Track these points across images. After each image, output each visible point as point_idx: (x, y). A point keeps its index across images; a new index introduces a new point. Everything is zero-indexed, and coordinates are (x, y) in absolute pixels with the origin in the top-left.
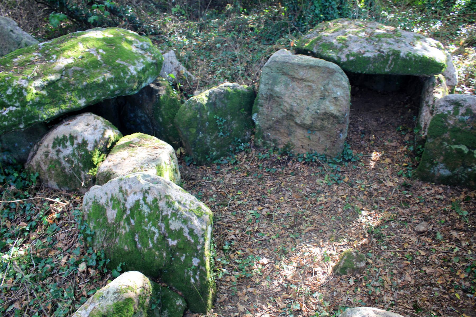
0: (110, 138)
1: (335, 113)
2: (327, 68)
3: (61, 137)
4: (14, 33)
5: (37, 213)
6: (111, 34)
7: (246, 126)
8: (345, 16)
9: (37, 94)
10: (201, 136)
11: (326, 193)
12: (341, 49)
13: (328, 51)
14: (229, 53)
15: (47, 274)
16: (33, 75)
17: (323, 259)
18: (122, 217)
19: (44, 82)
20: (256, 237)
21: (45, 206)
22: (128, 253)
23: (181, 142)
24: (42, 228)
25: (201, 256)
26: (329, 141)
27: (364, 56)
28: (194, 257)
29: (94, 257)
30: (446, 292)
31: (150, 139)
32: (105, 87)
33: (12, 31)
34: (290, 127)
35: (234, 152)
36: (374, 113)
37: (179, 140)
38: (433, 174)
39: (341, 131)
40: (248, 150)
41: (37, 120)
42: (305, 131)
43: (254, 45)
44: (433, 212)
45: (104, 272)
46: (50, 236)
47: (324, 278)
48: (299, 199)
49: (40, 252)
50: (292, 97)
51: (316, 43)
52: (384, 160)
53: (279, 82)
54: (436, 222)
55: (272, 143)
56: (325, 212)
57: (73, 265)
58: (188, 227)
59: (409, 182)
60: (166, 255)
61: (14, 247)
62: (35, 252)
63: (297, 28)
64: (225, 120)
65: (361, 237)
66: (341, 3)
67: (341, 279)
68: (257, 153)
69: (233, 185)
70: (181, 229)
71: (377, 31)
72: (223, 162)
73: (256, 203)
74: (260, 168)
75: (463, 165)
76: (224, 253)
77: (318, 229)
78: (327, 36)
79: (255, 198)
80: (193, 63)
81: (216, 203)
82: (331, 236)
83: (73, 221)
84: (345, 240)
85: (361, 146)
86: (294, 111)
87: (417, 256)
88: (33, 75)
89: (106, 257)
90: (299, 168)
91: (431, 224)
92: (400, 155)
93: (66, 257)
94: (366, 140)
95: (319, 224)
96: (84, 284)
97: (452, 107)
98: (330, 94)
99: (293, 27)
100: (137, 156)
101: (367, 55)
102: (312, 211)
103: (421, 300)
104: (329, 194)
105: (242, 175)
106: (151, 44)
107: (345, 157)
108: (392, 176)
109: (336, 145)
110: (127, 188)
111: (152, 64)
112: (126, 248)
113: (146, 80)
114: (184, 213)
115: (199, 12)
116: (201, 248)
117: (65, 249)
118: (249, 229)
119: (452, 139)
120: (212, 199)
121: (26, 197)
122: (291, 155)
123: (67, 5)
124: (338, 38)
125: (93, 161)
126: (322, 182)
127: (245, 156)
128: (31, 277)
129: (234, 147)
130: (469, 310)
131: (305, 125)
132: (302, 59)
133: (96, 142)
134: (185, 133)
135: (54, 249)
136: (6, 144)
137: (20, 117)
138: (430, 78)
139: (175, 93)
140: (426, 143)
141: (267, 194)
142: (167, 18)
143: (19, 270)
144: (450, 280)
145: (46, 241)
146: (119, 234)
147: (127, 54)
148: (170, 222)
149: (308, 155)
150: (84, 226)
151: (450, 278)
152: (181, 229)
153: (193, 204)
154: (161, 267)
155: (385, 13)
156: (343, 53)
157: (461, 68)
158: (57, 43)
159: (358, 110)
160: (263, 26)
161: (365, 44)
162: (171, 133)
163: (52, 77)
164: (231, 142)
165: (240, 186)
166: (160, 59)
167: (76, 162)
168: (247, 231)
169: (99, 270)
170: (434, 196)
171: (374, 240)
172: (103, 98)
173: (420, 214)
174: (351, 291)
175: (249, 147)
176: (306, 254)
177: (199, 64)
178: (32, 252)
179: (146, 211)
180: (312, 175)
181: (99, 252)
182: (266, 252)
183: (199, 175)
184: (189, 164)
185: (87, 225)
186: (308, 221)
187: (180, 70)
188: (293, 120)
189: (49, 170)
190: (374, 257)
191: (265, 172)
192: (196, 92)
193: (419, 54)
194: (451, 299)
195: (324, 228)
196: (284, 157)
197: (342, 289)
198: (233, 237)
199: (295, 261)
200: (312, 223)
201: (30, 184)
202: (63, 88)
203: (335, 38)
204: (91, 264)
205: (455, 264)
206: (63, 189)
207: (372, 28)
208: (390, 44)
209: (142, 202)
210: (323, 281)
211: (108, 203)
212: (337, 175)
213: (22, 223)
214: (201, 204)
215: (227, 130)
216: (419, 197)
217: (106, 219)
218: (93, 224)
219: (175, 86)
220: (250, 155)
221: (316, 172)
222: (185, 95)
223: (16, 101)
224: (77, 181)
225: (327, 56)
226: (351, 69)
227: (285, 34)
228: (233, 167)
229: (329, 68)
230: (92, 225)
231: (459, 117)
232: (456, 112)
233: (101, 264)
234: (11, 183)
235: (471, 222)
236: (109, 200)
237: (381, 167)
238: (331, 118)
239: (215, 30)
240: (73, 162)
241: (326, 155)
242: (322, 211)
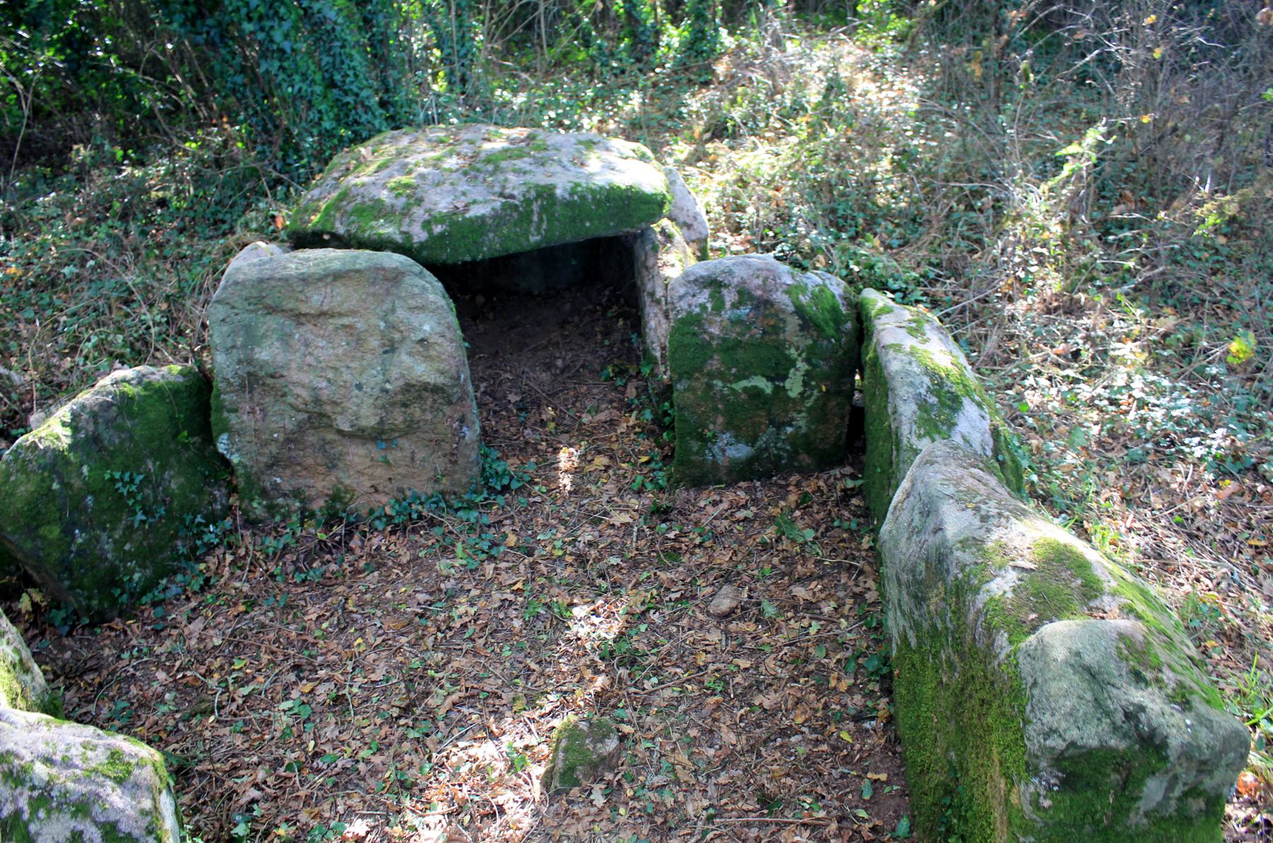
1: (433, 378)
2: (379, 269)
7: (206, 477)
8: (404, 120)
10: (80, 541)
11: (469, 591)
12: (406, 212)
13: (373, 223)
17: (511, 767)
20: (319, 771)
23: (25, 572)
27: (467, 215)
30: (820, 737)
34: (327, 447)
36: (536, 350)
38: (714, 463)
39: (462, 420)
40: (232, 539)
42: (369, 446)
43: (179, 245)
44: (740, 556)
47: (526, 814)
48: (404, 630)
50: (310, 365)
51: (338, 209)
52: (590, 462)
53: (264, 336)
54: (752, 577)
55: (290, 502)
56: (482, 641)
58: (96, 823)
59: (664, 501)
64: (141, 477)
65: (588, 674)
66: (387, 91)
67: (570, 802)
69: (215, 647)
71: (487, 146)
73: (292, 677)
74: (278, 578)
75: (772, 422)
77: (476, 692)
78: (363, 185)
79: (287, 665)
84: (551, 697)
85: (527, 443)
87: (733, 674)
90: (383, 548)
91: (741, 586)
92: (626, 440)
94: (535, 424)
95: (475, 677)
97: (707, 293)
98: (405, 334)
99: (275, 174)
101: (476, 211)
102: (448, 651)
103: (771, 780)
105: (233, 612)
107: (492, 483)
108: (622, 498)
109: (461, 461)
114: (70, 785)
118: (293, 755)
119: (730, 369)
120: (164, 709)
122: (352, 519)
124: (392, 184)
126: (453, 567)
127: (229, 558)
130: (877, 758)
131: (363, 431)
132: (308, 260)
134: (29, 545)
138: (642, 234)
140: (675, 395)
141: (314, 644)
144: (820, 706)
148: (33, 828)
151: (818, 701)
153: (94, 748)
155: (505, 93)
156: (412, 221)
157: (710, 194)
161: (463, 187)
164: (177, 532)
165: (237, 646)
168: (287, 762)
170: (732, 515)
171: (623, 672)
173: (712, 569)
174: (604, 823)
175: (233, 531)
176: (464, 769)
177: (24, 333)
180: (421, 554)
182: (355, 801)
183: (107, 652)
184: (67, 629)
186: (443, 681)
188: (331, 426)
190: (636, 714)
191: (295, 584)
192: (33, 418)
193: (600, 184)
194: (835, 748)
195: (491, 685)
196: (335, 529)
197: (580, 827)
198: (254, 793)
199: (441, 797)
200: (455, 682)
203: (384, 186)
205: (820, 663)
207: (472, 142)
208: (525, 173)
210: (527, 823)
212: (483, 536)
214: (121, 742)
215: (156, 501)
216: (698, 530)
220: (242, 552)
221: (430, 543)
225: (375, 237)
226: (444, 256)
227: (258, 200)
228: (200, 598)
229: (383, 269)
231: (727, 314)
232: (719, 306)
235: (826, 552)
237: (589, 482)
238: (426, 394)
239: (52, 226)
241: (442, 493)
242: (473, 640)
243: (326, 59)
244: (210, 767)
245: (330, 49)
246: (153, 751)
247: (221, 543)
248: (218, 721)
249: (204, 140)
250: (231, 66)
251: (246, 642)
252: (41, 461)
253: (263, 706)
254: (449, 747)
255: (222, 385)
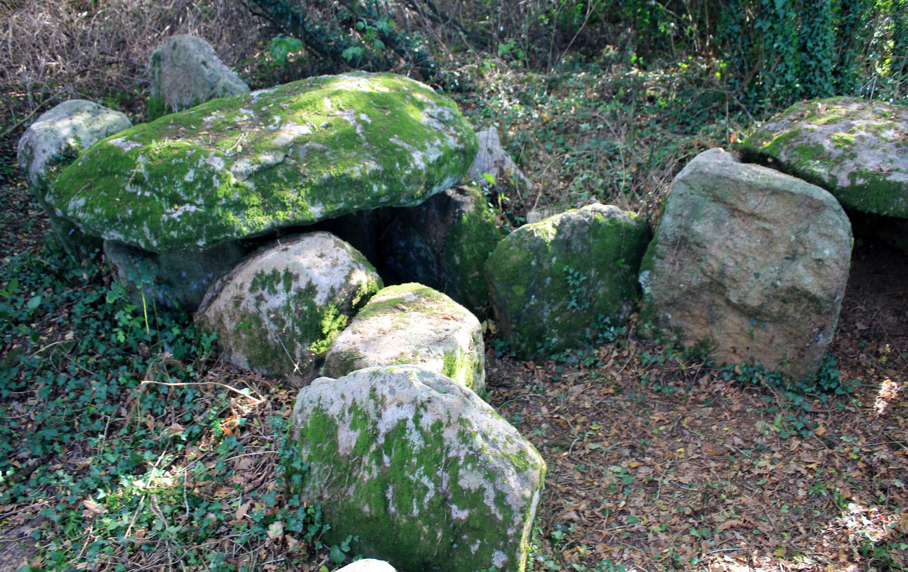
0: (359, 286)
1: (815, 290)
2: (809, 196)
3: (268, 272)
4: (208, 68)
5: (205, 410)
6: (385, 85)
8: (846, 89)
9: (237, 186)
10: (532, 303)
12: (839, 161)
13: (811, 162)
14: (604, 143)
15: (208, 531)
16: (235, 149)
18: (367, 447)
19: (252, 165)
21: (221, 400)
22: (369, 520)
23: (492, 308)
24: (209, 440)
25: (512, 550)
26: (793, 345)
27: (888, 179)
28: (498, 549)
29: (301, 516)
31: (438, 298)
32: (362, 187)
33: (204, 63)
34: (714, 308)
35: (594, 342)
37: (488, 304)
39: (822, 329)
40: (622, 342)
41: (229, 235)
42: (744, 319)
45: (316, 548)
46: (221, 458)
48: (715, 457)
49: (200, 487)
50: (727, 247)
51: (786, 143)
53: (704, 215)
56: (770, 493)
57: (259, 523)
60: (443, 536)
61: (155, 469)
62: (192, 486)
63: (743, 106)
64: (584, 278)
65: (844, 557)
68: (639, 351)
69: (584, 408)
70: (481, 490)
72: (570, 361)
73: (627, 452)
74: (643, 382)
76: (552, 546)
77: (751, 526)
78: (813, 131)
80: (531, 155)
81: (546, 441)
82: (777, 547)
83: (268, 438)
85: (859, 364)
86: (727, 277)
88: (235, 149)
89: (323, 520)
90: (722, 394)
93: (247, 506)
94: (871, 352)
95: (754, 516)
96: (274, 563)
98: (808, 251)
99: (736, 102)
100: (409, 330)
102: (741, 487)
104: (780, 456)
105: (604, 390)
106: (460, 114)
107: (822, 382)
109: (807, 357)
110: (386, 392)
111: (457, 151)
112: (366, 509)
113: (441, 180)
114: (491, 458)
115: (550, 55)
116: (515, 534)
117: (246, 489)
118: (608, 505)
120: (538, 432)
121: (188, 378)
122: (709, 364)
123: (304, 22)
125: (322, 327)
126: (768, 429)
127: (615, 354)
128: (178, 533)
129: (594, 333)
131: (746, 307)
132: (758, 173)
133: (332, 290)
135: (227, 485)
136: (165, 271)
137: (201, 226)
139: (491, 214)
141: (650, 438)
142: (486, 63)
143: (159, 515)
145: (213, 466)
146: (356, 478)
147: (412, 127)
148: (461, 472)
149: (745, 369)
150: (291, 452)
152: (481, 490)
153: (512, 443)
154: (429, 558)
156: (842, 169)
158: (284, 93)
159: (858, 287)
160: (674, 96)
161: (892, 155)
162: (474, 288)
163: (267, 158)
164: (590, 323)
165: (599, 414)
166: (473, 143)
167: (289, 323)
168: (602, 507)
169: (306, 542)
172: (356, 207)
177: (541, 158)
178: (185, 484)
179: (417, 443)
180: (749, 410)
181: (311, 506)
182: (637, 556)
183: (518, 379)
184: (500, 354)
185: (297, 451)
187: (505, 168)
188: (723, 295)
189: (237, 332)
191: (652, 391)
192: (532, 214)
195: (764, 527)
196: (694, 365)
198: (574, 516)
200: (738, 512)
201: (198, 353)
202: (286, 180)
203: (828, 137)
204: (293, 529)
206: (256, 370)
209: (410, 424)
211: (343, 415)
213: (175, 426)
215: (586, 297)
217: (335, 445)
218: (309, 452)
219: (493, 198)
220: (625, 353)
221: (758, 405)
222: (511, 217)
223: (198, 195)
224: (285, 361)
225: (809, 172)
226: (857, 203)
228: (587, 372)
229: (812, 198)
230: (306, 453)
233: (313, 530)
234: (166, 347)
236: (347, 410)
237: (900, 415)
240: (284, 322)
241: (782, 374)
242: (763, 489)
243: (806, 29)
244: (554, 484)
245: (812, 22)
246: (543, 462)
247: (614, 341)
248: (569, 457)
249: (693, 64)
250: (734, 18)
251: (606, 414)
252: (532, 244)
253: (601, 462)
254: (717, 555)
255: (661, 238)
